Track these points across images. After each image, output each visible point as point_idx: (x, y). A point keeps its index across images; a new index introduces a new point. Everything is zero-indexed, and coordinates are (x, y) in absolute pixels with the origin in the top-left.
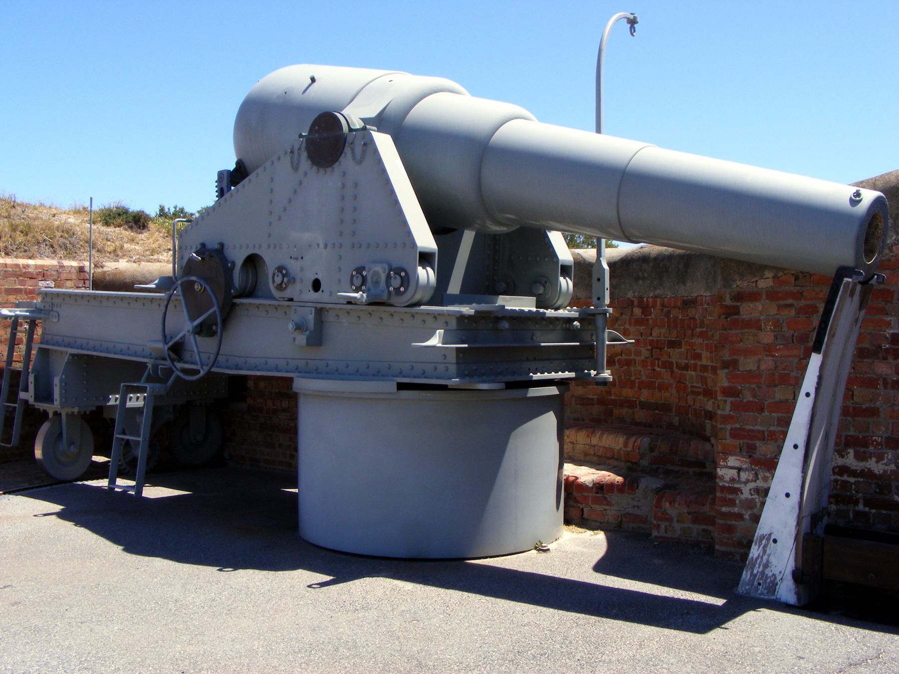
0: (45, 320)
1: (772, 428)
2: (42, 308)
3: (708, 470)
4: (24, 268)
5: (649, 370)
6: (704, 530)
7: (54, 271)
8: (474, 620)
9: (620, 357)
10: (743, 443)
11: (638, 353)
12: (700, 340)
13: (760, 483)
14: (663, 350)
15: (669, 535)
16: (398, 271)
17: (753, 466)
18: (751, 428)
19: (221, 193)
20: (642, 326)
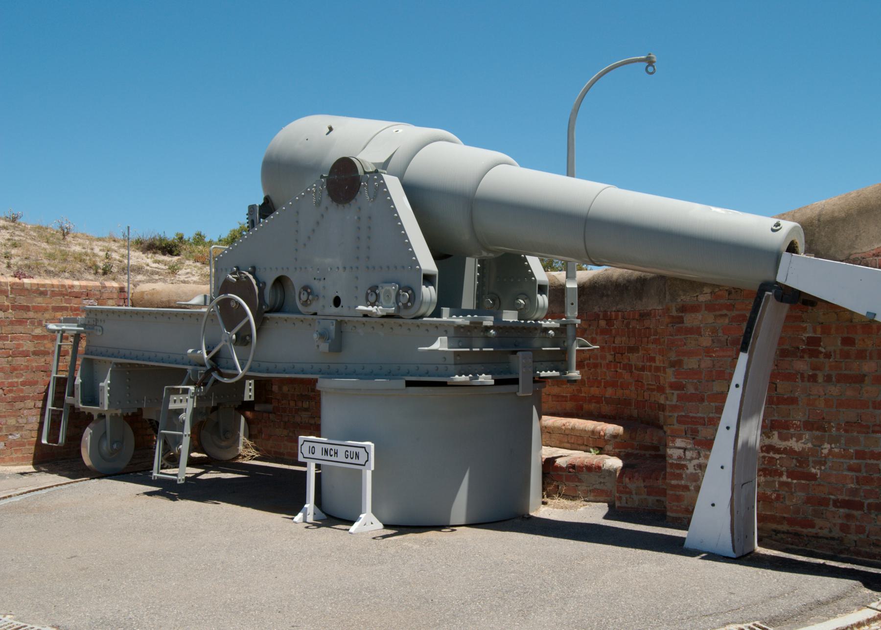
0: (89, 334)
1: (711, 415)
2: (87, 323)
3: (661, 453)
4: (70, 288)
5: (612, 371)
6: (657, 501)
7: (98, 291)
8: (469, 569)
9: (588, 361)
10: (688, 427)
11: (603, 358)
12: (654, 346)
13: (702, 460)
14: (624, 355)
15: (629, 505)
16: (407, 289)
17: (696, 446)
18: (694, 415)
19: (252, 224)
20: (606, 335)
